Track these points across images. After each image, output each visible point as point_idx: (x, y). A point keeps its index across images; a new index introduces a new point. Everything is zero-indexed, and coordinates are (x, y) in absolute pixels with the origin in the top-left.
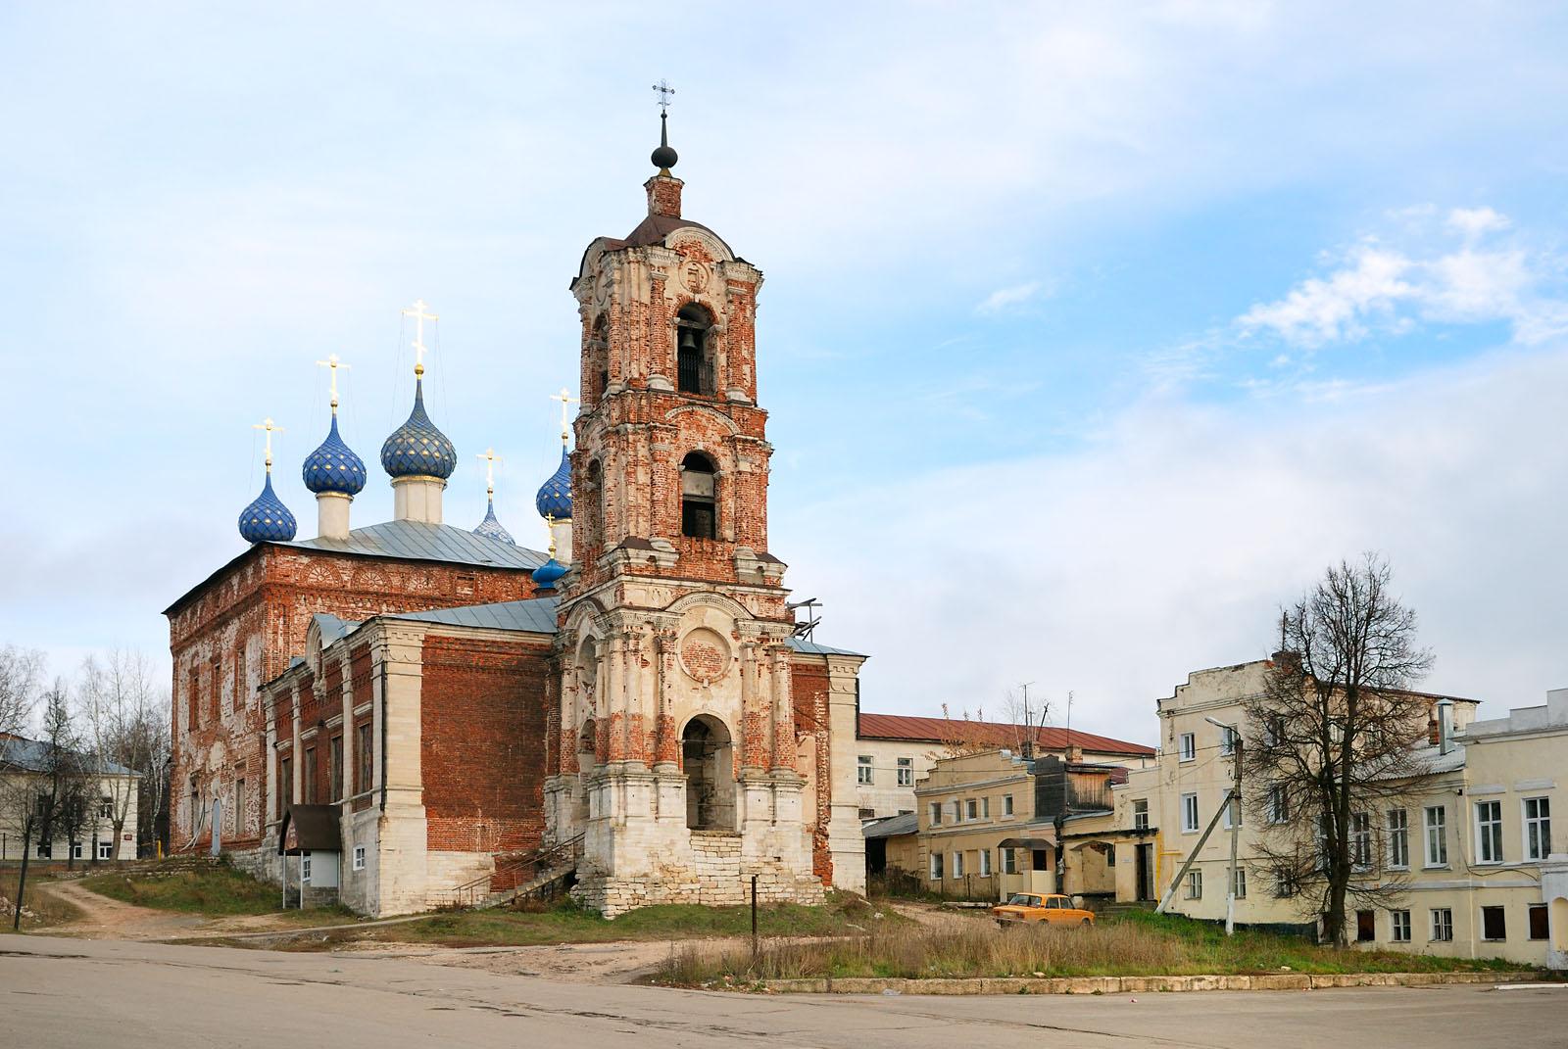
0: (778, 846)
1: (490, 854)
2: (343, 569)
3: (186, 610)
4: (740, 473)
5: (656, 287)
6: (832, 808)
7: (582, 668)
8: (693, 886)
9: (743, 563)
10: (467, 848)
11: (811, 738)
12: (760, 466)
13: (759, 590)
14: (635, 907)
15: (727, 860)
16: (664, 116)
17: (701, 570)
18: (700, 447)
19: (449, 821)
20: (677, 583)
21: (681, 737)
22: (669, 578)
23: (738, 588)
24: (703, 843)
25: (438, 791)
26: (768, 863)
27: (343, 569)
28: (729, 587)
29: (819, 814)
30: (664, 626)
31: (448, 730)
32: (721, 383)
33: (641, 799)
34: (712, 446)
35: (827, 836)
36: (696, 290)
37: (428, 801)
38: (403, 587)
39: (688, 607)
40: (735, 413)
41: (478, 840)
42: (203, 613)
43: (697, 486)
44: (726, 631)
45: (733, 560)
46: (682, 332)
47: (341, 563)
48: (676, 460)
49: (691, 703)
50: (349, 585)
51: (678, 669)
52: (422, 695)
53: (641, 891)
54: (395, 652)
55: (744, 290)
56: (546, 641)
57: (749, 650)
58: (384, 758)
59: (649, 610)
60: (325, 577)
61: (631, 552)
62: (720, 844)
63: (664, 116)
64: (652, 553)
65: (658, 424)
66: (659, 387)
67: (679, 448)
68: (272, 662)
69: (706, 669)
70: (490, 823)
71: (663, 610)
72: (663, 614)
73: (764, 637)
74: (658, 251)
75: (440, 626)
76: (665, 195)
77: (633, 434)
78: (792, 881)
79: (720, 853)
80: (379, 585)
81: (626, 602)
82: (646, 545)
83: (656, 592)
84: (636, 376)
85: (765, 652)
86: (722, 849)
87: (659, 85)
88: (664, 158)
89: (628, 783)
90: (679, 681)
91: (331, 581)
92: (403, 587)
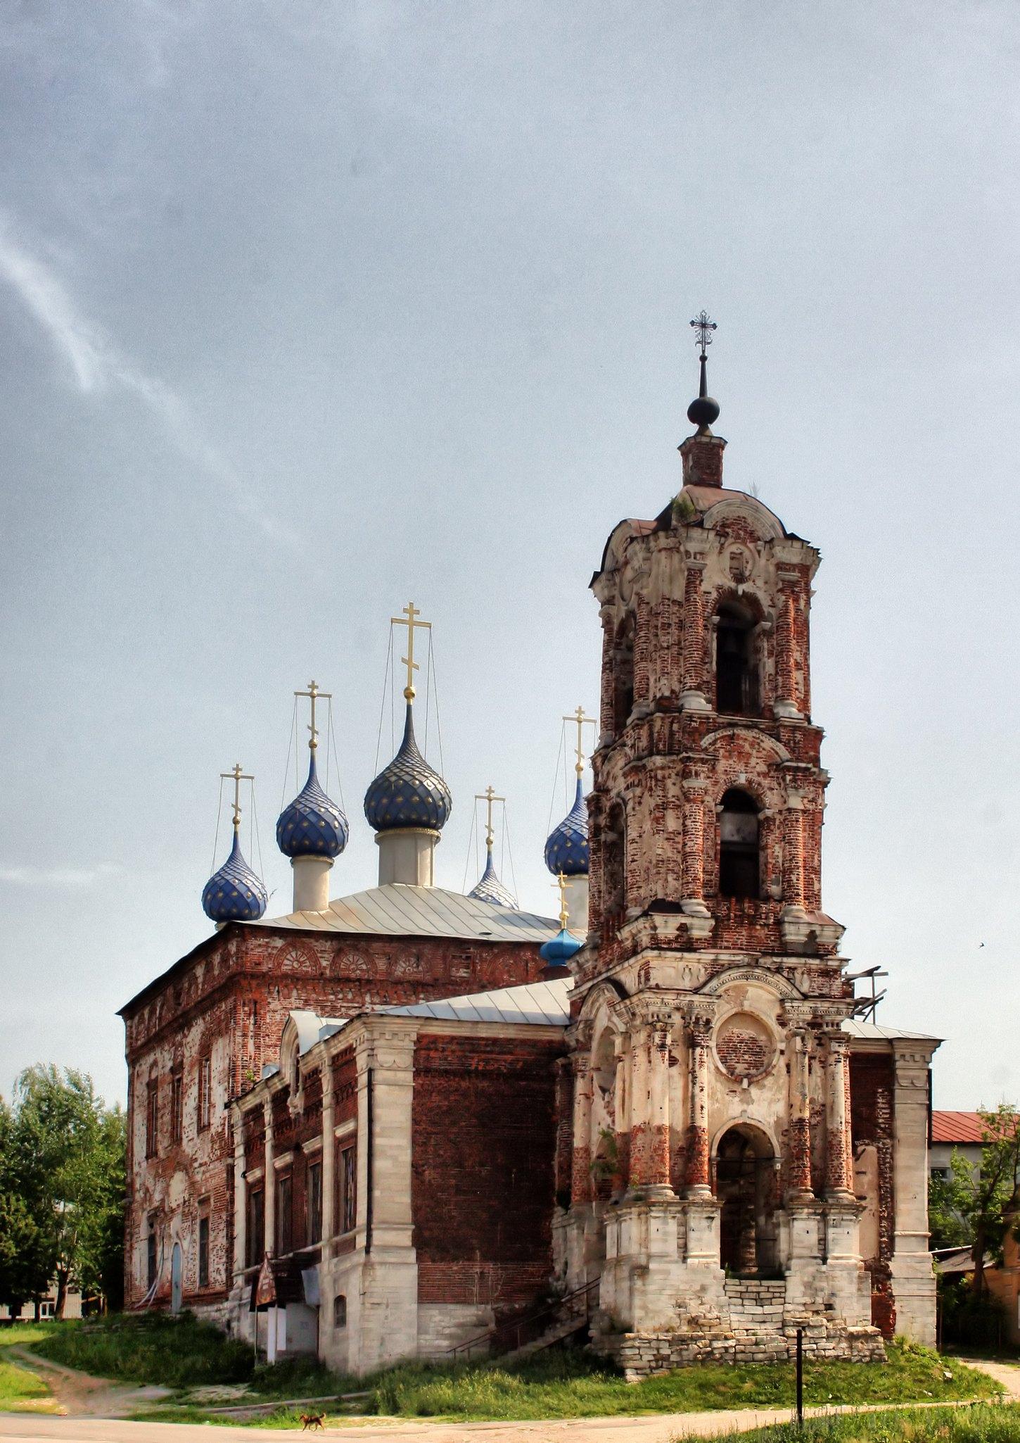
1: (489, 1307)
2: (322, 951)
3: (143, 1008)
4: (789, 810)
5: (694, 577)
7: (598, 1069)
11: (872, 1149)
15: (768, 1309)
18: (742, 780)
19: (442, 1266)
23: (785, 959)
24: (739, 1288)
25: (431, 1230)
27: (322, 951)
32: (766, 693)
33: (665, 1233)
34: (756, 779)
36: (740, 578)
37: (420, 1242)
38: (389, 973)
41: (476, 1289)
44: (770, 1016)
46: (721, 630)
48: (712, 801)
50: (328, 972)
51: (712, 1067)
52: (413, 1109)
54: (384, 1057)
57: (798, 1039)
60: (301, 963)
61: (658, 919)
64: (684, 920)
65: (690, 754)
68: (241, 1071)
69: (746, 1064)
70: (490, 1267)
71: (696, 991)
73: (815, 1024)
75: (435, 1023)
76: (703, 459)
77: (662, 768)
79: (759, 1301)
80: (362, 970)
81: (652, 983)
84: (667, 694)
86: (763, 1295)
87: (698, 320)
88: (703, 412)
89: (653, 1214)
91: (307, 968)
92: (389, 973)
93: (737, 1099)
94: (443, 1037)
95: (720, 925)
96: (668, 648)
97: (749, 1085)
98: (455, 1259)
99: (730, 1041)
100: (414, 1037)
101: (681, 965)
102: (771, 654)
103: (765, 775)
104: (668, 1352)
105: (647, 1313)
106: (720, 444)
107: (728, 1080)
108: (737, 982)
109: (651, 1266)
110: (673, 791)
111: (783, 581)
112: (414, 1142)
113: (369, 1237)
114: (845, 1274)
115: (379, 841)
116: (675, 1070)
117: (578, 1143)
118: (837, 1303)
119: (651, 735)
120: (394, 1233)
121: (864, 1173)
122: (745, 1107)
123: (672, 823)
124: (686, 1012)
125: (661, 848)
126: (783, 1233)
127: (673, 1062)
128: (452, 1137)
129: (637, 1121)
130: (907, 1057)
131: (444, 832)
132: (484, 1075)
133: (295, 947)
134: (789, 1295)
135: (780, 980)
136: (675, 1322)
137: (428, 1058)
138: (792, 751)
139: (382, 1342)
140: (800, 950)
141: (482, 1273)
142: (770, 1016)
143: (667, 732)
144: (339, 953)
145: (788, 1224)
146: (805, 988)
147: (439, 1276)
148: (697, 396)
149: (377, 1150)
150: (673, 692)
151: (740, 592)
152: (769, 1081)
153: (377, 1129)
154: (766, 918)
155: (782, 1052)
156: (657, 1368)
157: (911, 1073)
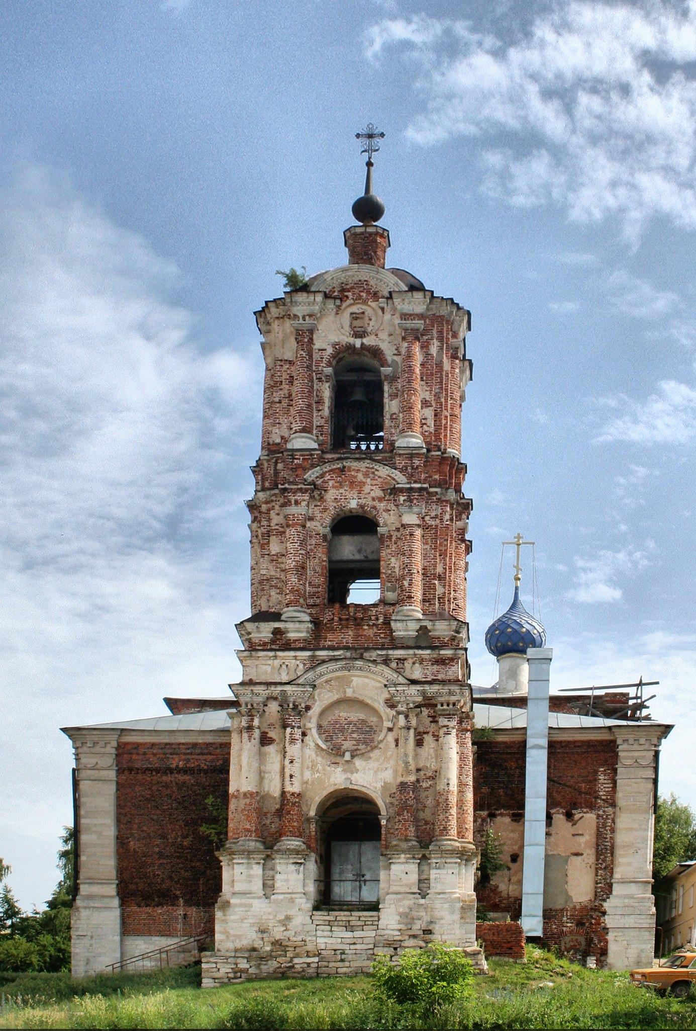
0: (427, 918)
6: (615, 886)
8: (309, 960)
9: (399, 625)
10: (169, 935)
13: (420, 652)
16: (369, 164)
17: (348, 636)
18: (353, 504)
19: (149, 910)
20: (308, 653)
23: (390, 652)
28: (379, 652)
29: (596, 892)
30: (292, 699)
31: (145, 828)
33: (250, 876)
35: (604, 913)
41: (180, 926)
43: (359, 551)
44: (378, 702)
48: (321, 525)
49: (329, 778)
51: (312, 745)
59: (268, 684)
62: (351, 918)
63: (369, 164)
65: (287, 486)
67: (325, 510)
69: (348, 737)
72: (288, 688)
75: (133, 733)
77: (267, 503)
79: (349, 927)
83: (284, 667)
84: (278, 440)
85: (431, 719)
86: (352, 923)
88: (368, 209)
90: (314, 755)
94: (145, 744)
96: (280, 402)
97: (353, 757)
98: (160, 904)
99: (336, 723)
100: (115, 744)
101: (277, 662)
103: (380, 500)
104: (248, 966)
105: (228, 937)
107: (329, 754)
114: (446, 906)
118: (436, 928)
120: (99, 886)
122: (349, 775)
128: (155, 817)
130: (631, 741)
132: (185, 771)
134: (382, 924)
135: (387, 671)
136: (258, 944)
137: (130, 761)
139: (88, 962)
140: (412, 643)
141: (185, 915)
142: (378, 702)
145: (388, 867)
146: (417, 674)
147: (144, 916)
150: (282, 437)
152: (375, 754)
153: (82, 812)
154: (377, 619)
155: (390, 730)
156: (235, 978)
157: (636, 754)
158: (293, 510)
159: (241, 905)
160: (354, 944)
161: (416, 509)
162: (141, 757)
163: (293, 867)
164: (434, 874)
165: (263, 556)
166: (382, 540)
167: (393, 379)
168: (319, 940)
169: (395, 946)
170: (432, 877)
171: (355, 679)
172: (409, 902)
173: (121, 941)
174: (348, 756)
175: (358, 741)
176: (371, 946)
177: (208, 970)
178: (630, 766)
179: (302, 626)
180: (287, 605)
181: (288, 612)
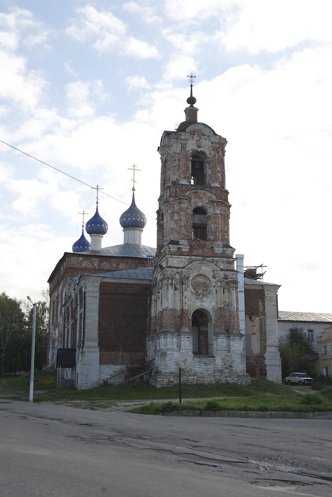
4: (216, 214)
5: (183, 147)
8: (194, 377)
11: (257, 319)
12: (225, 211)
13: (223, 259)
14: (169, 386)
15: (209, 367)
16: (191, 86)
17: (200, 252)
18: (200, 205)
19: (109, 353)
20: (189, 257)
21: (191, 318)
22: (186, 255)
23: (214, 258)
24: (199, 360)
26: (227, 368)
33: (172, 342)
34: (205, 204)
37: (100, 345)
39: (194, 266)
40: (214, 192)
41: (120, 360)
42: (55, 280)
45: (212, 248)
46: (193, 163)
47: (94, 259)
48: (190, 211)
50: (97, 267)
51: (190, 291)
53: (172, 379)
54: (89, 289)
55: (218, 146)
56: (147, 283)
57: (219, 282)
58: (84, 329)
59: (177, 268)
61: (171, 246)
63: (191, 86)
64: (179, 246)
66: (183, 183)
69: (201, 289)
70: (125, 354)
71: (183, 268)
72: (183, 270)
73: (226, 277)
74: (183, 133)
76: (192, 113)
77: (173, 201)
78: (236, 375)
79: (206, 364)
81: (169, 265)
82: (177, 243)
84: (175, 180)
86: (207, 362)
87: (190, 75)
88: (191, 100)
89: (168, 336)
91: (90, 266)
93: (198, 301)
95: (191, 247)
97: (203, 296)
100: (100, 282)
102: (210, 168)
103: (208, 204)
104: (173, 380)
106: (196, 110)
108: (199, 265)
109: (167, 352)
110: (176, 208)
111: (214, 147)
112: (99, 314)
113: (83, 344)
115: (124, 231)
116: (177, 292)
117: (153, 315)
118: (233, 365)
119: (170, 192)
121: (255, 326)
123: (176, 217)
124: (180, 274)
125: (173, 225)
126: (215, 343)
127: (176, 289)
129: (164, 307)
131: (144, 229)
133: (86, 260)
138: (217, 197)
140: (220, 256)
143: (174, 191)
144: (101, 262)
146: (222, 267)
147: (107, 356)
148: (190, 96)
149: (86, 317)
151: (199, 150)
152: (210, 295)
153: (87, 310)
155: (214, 286)
157: (271, 295)
158: (183, 205)
159: (171, 354)
160: (208, 371)
161: (220, 208)
162: (108, 288)
163: (187, 339)
164: (232, 343)
165: (172, 220)
166: (209, 217)
167: (209, 163)
168: (196, 369)
169: (221, 371)
170: (231, 344)
171: (203, 267)
172: (224, 353)
173: (100, 366)
174: (201, 296)
175: (203, 290)
176: (213, 372)
177: (160, 381)
178: (269, 300)
179: (187, 247)
180: (182, 239)
181: (181, 242)
